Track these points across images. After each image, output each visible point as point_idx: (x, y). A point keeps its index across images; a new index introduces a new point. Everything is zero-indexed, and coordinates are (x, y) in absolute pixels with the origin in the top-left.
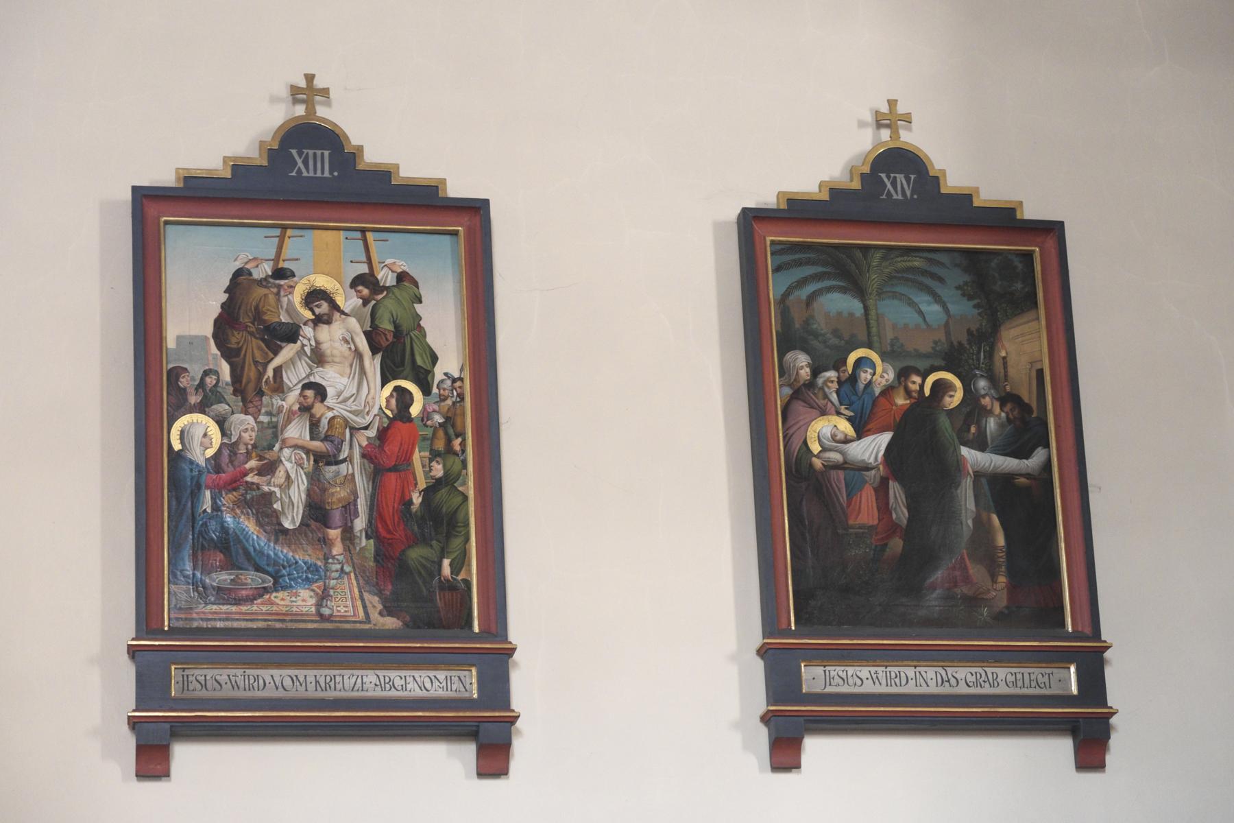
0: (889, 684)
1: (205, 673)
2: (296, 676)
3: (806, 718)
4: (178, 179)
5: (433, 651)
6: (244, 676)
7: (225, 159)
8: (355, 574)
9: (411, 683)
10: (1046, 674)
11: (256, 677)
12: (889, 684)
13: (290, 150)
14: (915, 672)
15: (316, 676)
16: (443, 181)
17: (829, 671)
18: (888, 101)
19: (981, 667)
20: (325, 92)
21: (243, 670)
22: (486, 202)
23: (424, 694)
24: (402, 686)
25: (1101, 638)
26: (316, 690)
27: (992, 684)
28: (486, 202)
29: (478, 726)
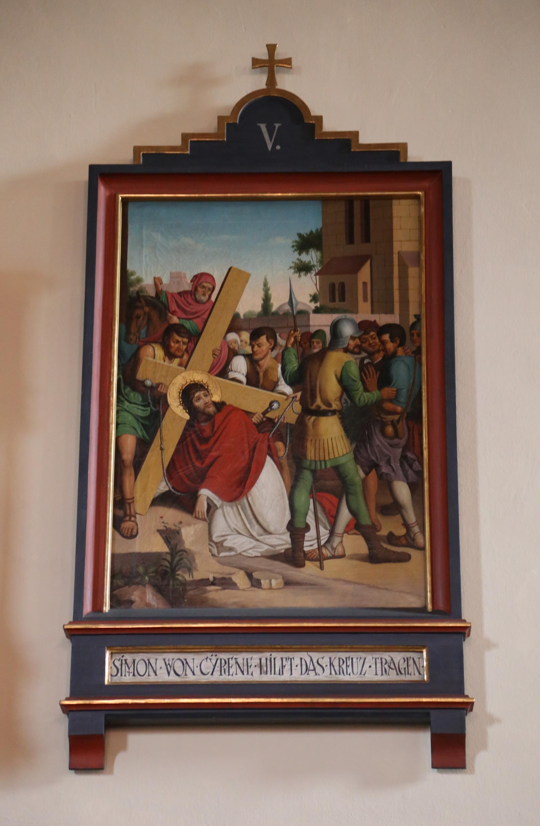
2: (186, 660)
5: (122, 632)
7: (185, 137)
8: (234, 556)
9: (234, 667)
13: (259, 124)
15: (164, 660)
16: (404, 146)
18: (267, 46)
21: (122, 655)
22: (448, 165)
23: (173, 678)
24: (405, 669)
25: (461, 618)
26: (331, 674)
27: (338, 673)
28: (448, 165)
29: (428, 714)
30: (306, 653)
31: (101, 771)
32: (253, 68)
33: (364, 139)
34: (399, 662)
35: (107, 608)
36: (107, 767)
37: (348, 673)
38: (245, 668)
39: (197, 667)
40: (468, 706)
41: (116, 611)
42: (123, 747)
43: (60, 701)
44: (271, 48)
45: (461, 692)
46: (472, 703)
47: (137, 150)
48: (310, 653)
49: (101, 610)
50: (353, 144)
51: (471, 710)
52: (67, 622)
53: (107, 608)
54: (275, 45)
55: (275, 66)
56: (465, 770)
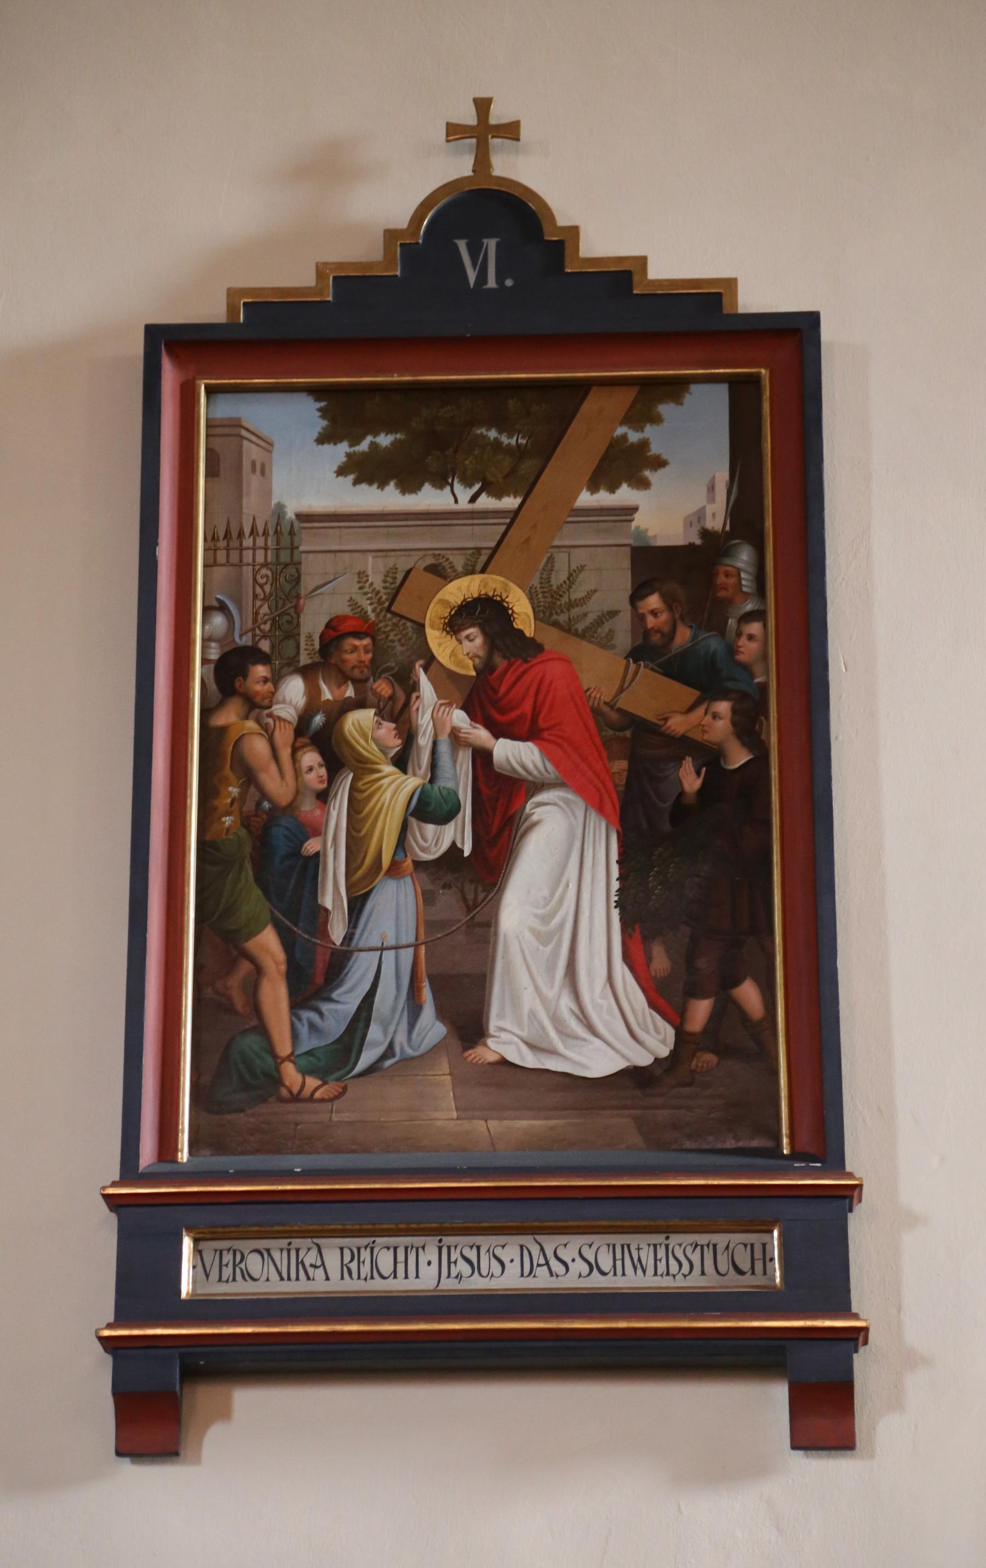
0: (293, 1275)
1: (713, 1242)
3: (183, 1350)
4: (232, 309)
6: (289, 1251)
10: (412, 1247)
11: (355, 1251)
12: (293, 1275)
14: (440, 1249)
16: (731, 284)
17: (449, 1248)
19: (312, 1237)
20: (511, 131)
22: (813, 319)
27: (285, 1275)
28: (813, 319)
30: (531, 1237)
31: (174, 1458)
32: (448, 141)
33: (656, 272)
34: (733, 1250)
35: (184, 1155)
36: (184, 1451)
37: (363, 1276)
38: (651, 1262)
39: (429, 1263)
40: (857, 1337)
41: (197, 1160)
42: (225, 1413)
43: (97, 1331)
44: (483, 105)
45: (844, 1309)
46: (865, 1330)
47: (233, 294)
48: (538, 1238)
49: (174, 1160)
50: (636, 278)
51: (866, 1342)
52: (109, 1183)
53: (184, 1155)
54: (449, 125)
55: (490, 136)
56: (853, 1452)
